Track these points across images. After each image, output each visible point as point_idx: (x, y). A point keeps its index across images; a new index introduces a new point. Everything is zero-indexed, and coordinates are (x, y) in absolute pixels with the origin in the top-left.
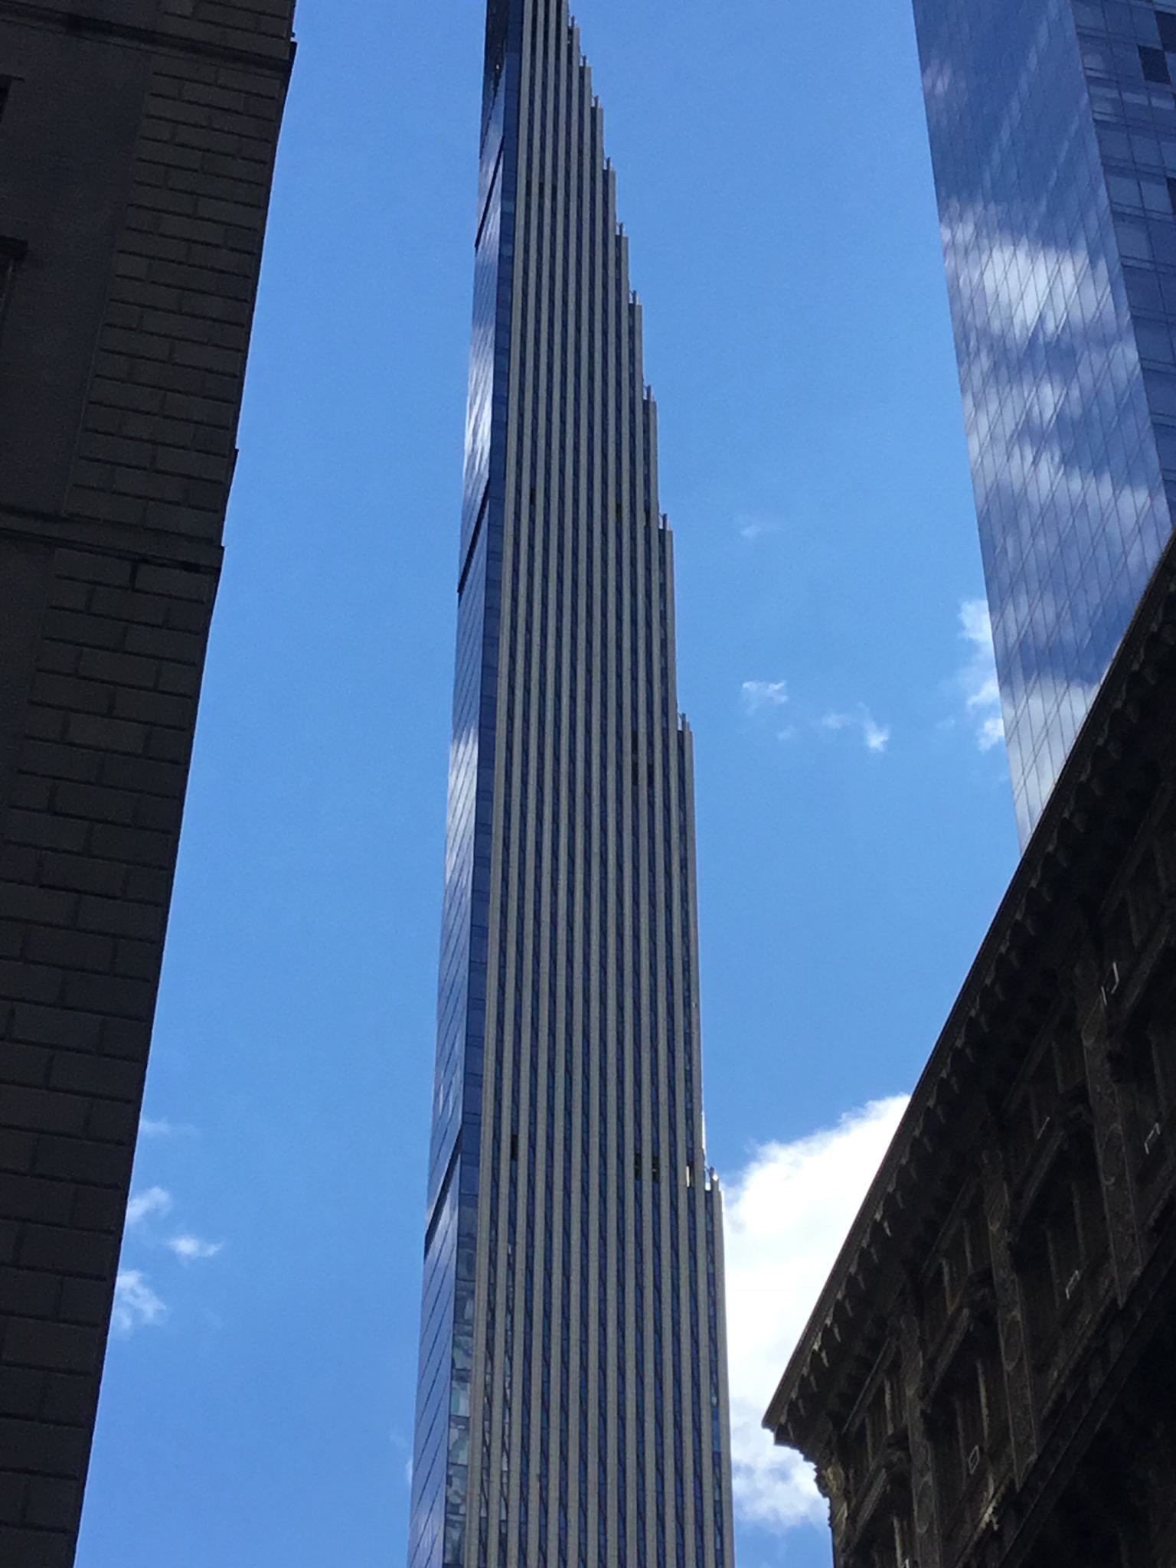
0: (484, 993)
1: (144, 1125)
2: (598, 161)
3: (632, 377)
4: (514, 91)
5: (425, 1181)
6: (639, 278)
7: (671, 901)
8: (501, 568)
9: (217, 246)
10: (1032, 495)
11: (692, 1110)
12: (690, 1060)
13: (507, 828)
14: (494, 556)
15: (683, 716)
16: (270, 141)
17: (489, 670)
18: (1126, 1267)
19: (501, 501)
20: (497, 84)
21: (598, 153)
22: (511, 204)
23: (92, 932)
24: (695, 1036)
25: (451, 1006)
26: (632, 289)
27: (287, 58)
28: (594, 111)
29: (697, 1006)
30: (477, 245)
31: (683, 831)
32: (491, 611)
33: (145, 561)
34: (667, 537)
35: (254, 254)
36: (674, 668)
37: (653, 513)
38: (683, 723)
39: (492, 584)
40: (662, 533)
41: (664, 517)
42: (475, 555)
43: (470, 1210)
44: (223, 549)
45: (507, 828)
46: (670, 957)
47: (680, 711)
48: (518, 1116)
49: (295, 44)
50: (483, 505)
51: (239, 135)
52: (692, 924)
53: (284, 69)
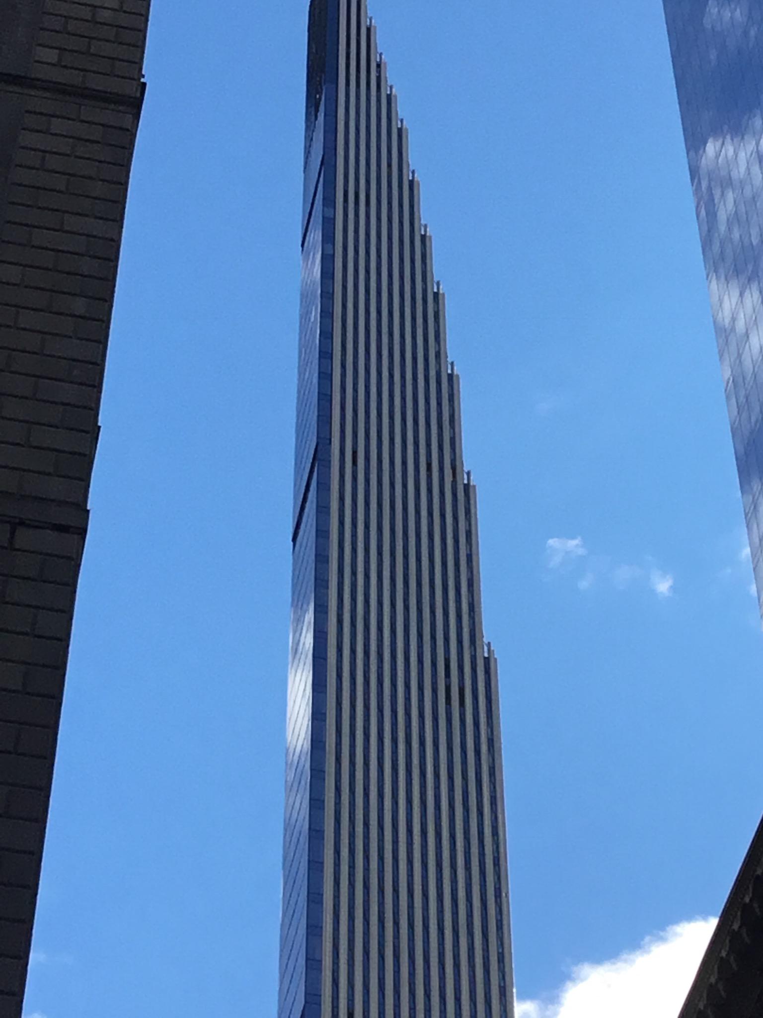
0: (326, 633)
1: (35, 957)
2: (405, 171)
3: (438, 355)
4: (331, 117)
5: (292, 502)
6: (442, 270)
7: (482, 807)
8: (330, 451)
9: (49, 474)
10: (734, 175)
11: (504, 987)
12: (502, 944)
13: (339, 744)
14: (323, 509)
15: (489, 644)
16: (125, 166)
17: (314, 929)
18: (757, 409)
19: (328, 464)
20: (317, 111)
21: (405, 166)
22: (330, 246)
23: (44, 425)
24: (505, 922)
25: (294, 894)
26: (436, 279)
27: (138, 95)
28: (400, 131)
29: (507, 896)
30: (294, 539)
31: (491, 742)
32: (321, 558)
33: (22, 523)
34: (471, 490)
35: (111, 259)
36: (480, 603)
37: (458, 470)
38: (489, 650)
39: (322, 533)
40: (467, 487)
41: (468, 474)
42: (306, 510)
43: (327, 215)
44: (88, 511)
45: (339, 744)
46: (482, 854)
47: (485, 640)
48: (353, 995)
49: (144, 84)
50: (321, 169)
51: (103, 125)
52: (500, 824)
53: (135, 104)
